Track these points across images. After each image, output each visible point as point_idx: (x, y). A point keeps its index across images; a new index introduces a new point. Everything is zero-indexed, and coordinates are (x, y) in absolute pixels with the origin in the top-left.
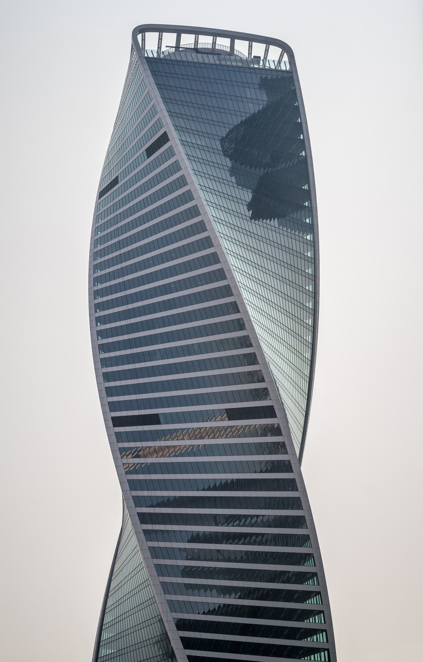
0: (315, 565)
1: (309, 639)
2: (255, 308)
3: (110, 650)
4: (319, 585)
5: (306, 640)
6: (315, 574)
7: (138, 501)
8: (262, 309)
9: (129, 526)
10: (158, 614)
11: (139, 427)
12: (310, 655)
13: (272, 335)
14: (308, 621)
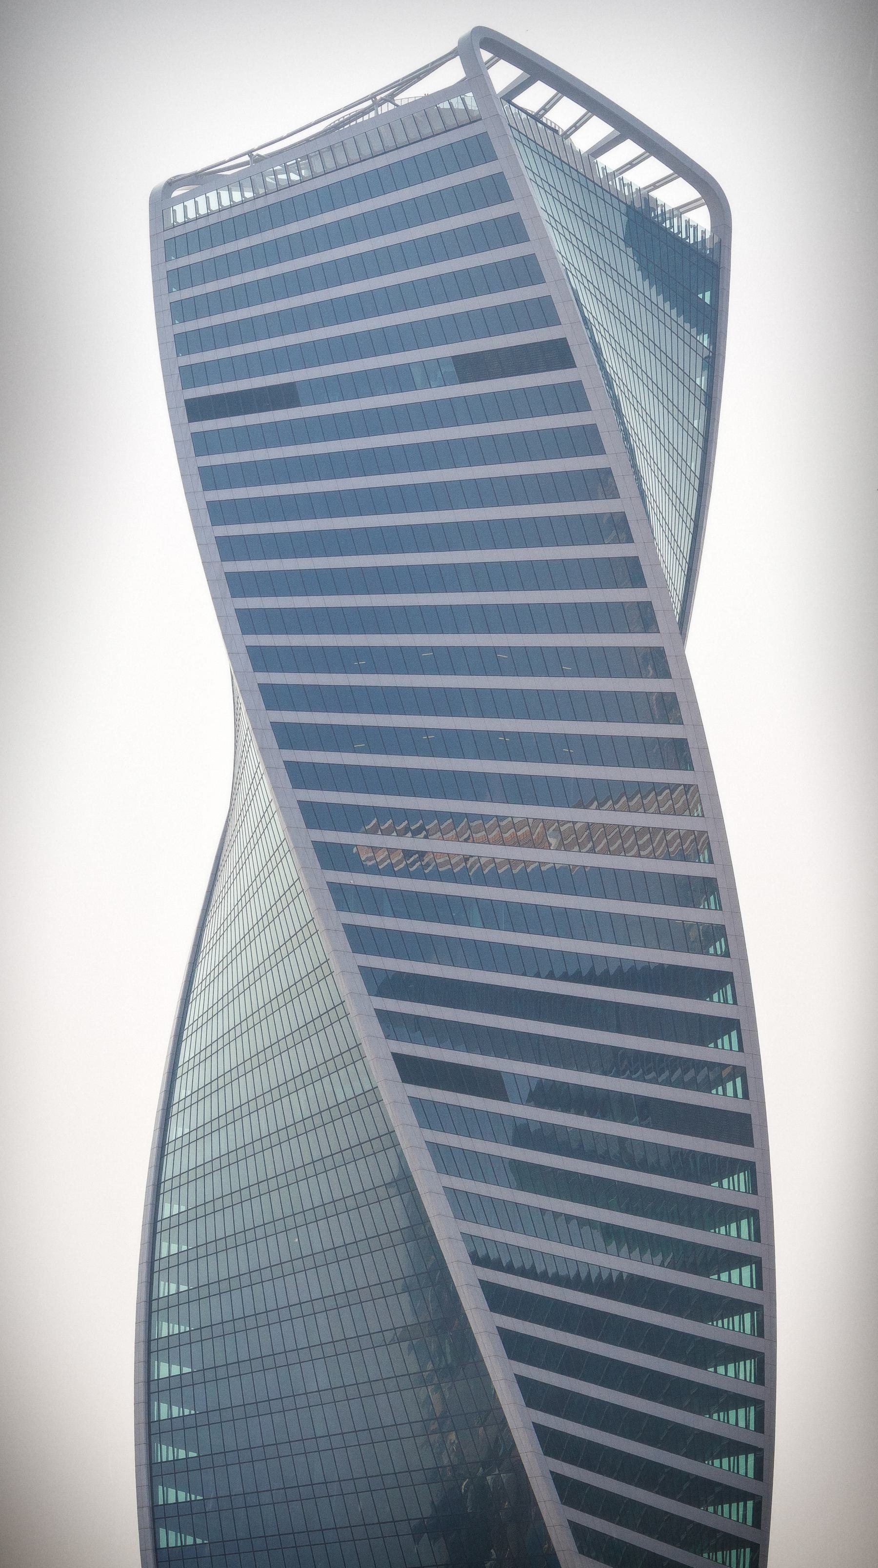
0: (735, 1002)
1: (725, 1182)
2: (640, 338)
3: (176, 1207)
4: (721, 909)
5: (723, 1230)
6: (739, 1072)
7: (273, 697)
8: (657, 343)
9: (254, 757)
10: (367, 1087)
11: (248, 417)
12: (726, 1223)
13: (670, 409)
14: (734, 1233)
